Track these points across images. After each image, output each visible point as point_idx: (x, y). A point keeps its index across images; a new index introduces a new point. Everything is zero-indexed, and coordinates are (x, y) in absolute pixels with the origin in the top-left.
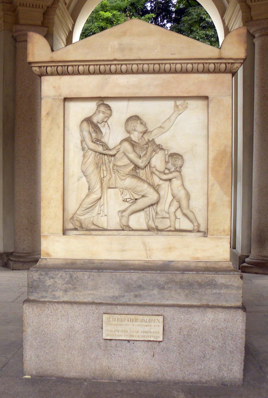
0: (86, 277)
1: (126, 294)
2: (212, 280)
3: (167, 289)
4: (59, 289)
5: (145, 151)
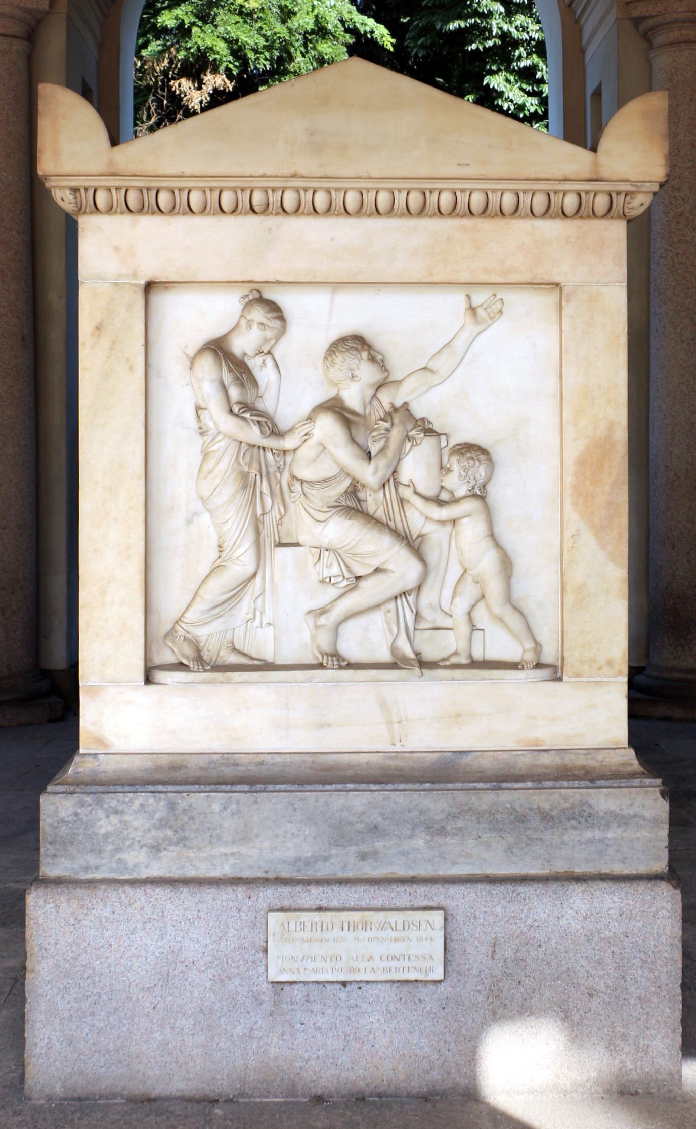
0: (216, 807)
1: (334, 851)
2: (582, 805)
3: (454, 834)
4: (136, 845)
5: (384, 440)
